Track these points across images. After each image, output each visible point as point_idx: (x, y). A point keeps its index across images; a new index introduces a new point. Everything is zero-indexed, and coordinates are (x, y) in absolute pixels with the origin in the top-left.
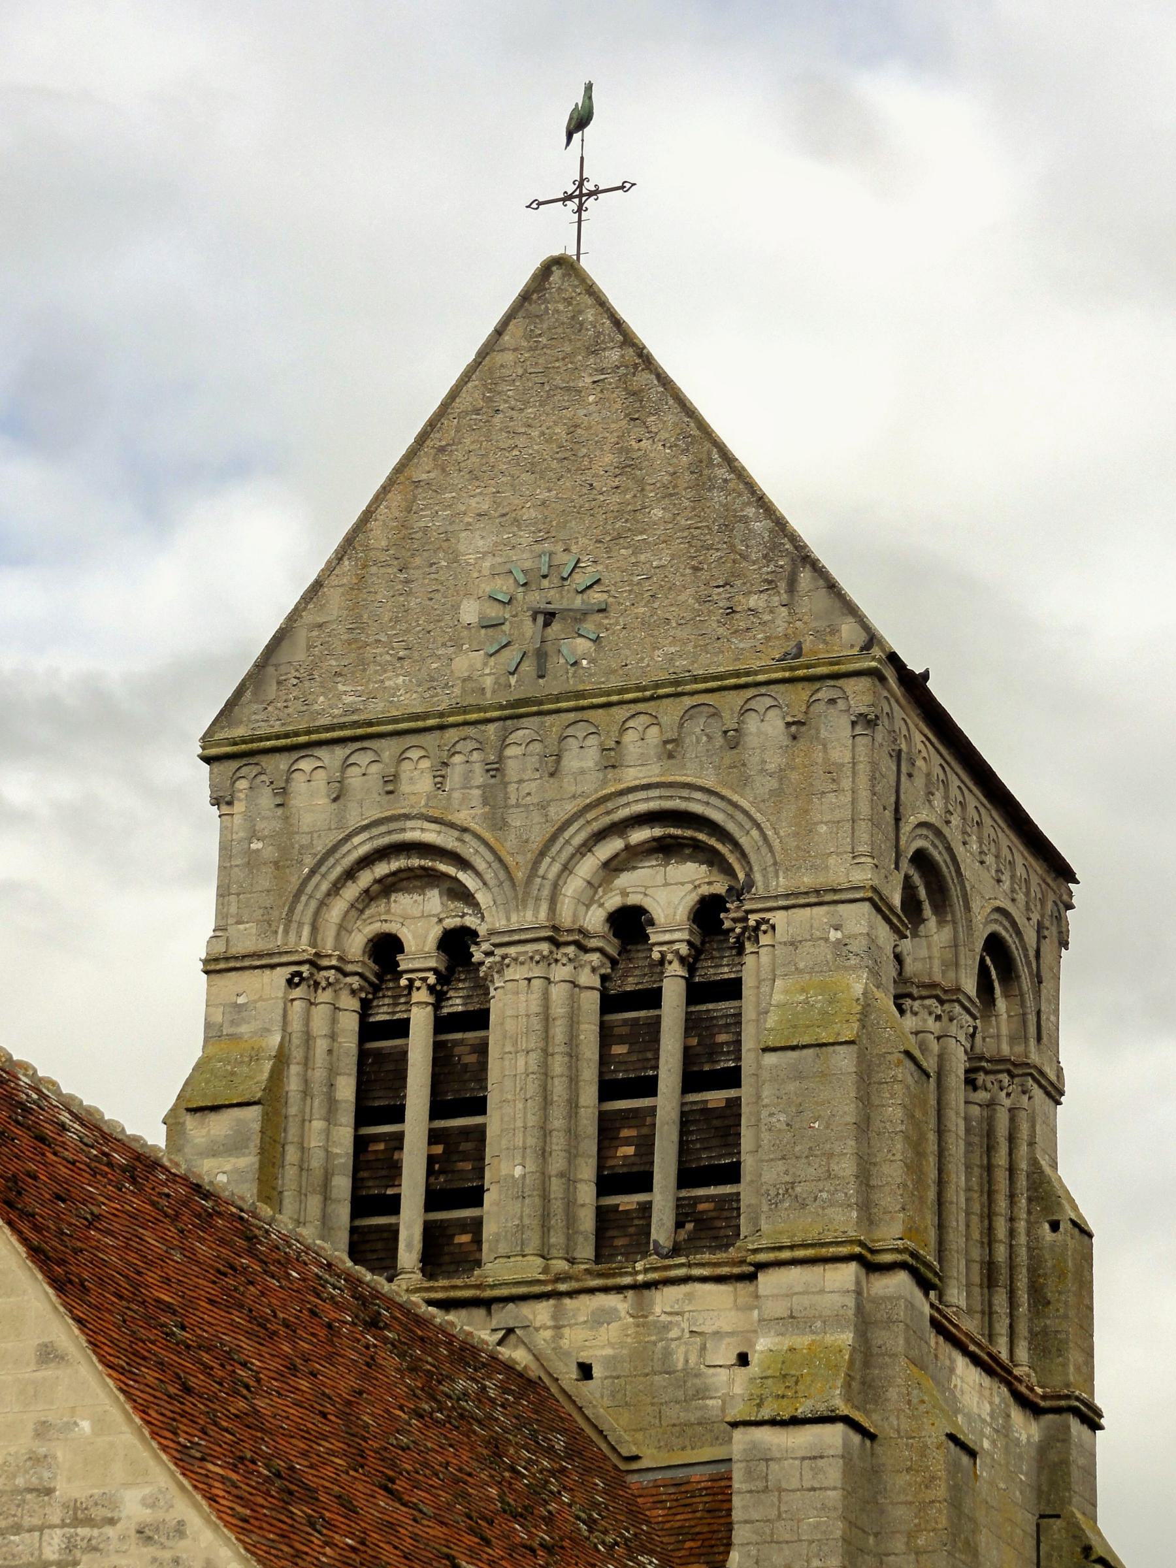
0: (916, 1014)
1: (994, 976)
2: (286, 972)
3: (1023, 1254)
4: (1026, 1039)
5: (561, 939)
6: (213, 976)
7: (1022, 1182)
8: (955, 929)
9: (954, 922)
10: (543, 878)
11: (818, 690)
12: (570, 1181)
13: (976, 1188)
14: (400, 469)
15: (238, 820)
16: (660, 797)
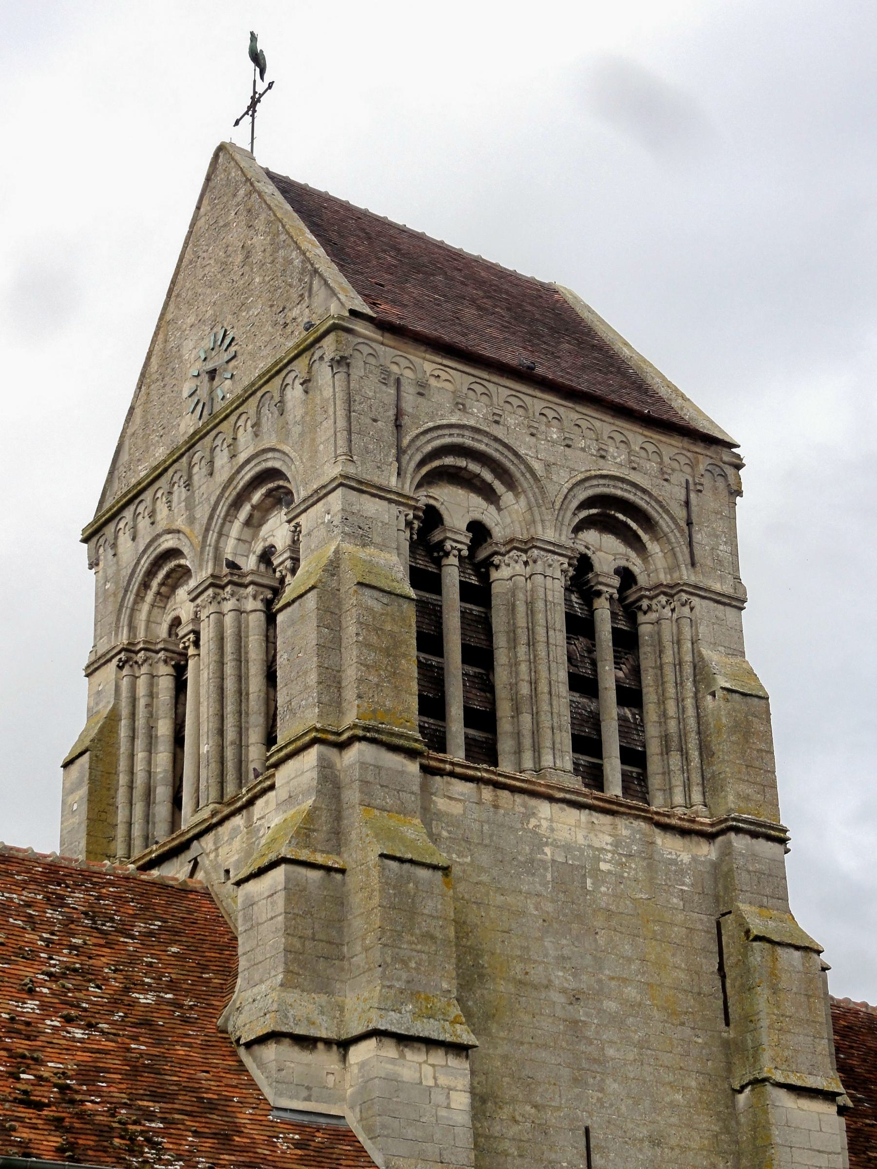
0: (508, 565)
1: (634, 525)
2: (115, 661)
3: (692, 722)
4: (679, 566)
5: (223, 583)
6: (91, 677)
7: (688, 670)
8: (527, 497)
9: (524, 492)
10: (210, 545)
11: (313, 355)
12: (241, 746)
13: (652, 683)
14: (161, 318)
15: (101, 573)
16: (255, 465)
